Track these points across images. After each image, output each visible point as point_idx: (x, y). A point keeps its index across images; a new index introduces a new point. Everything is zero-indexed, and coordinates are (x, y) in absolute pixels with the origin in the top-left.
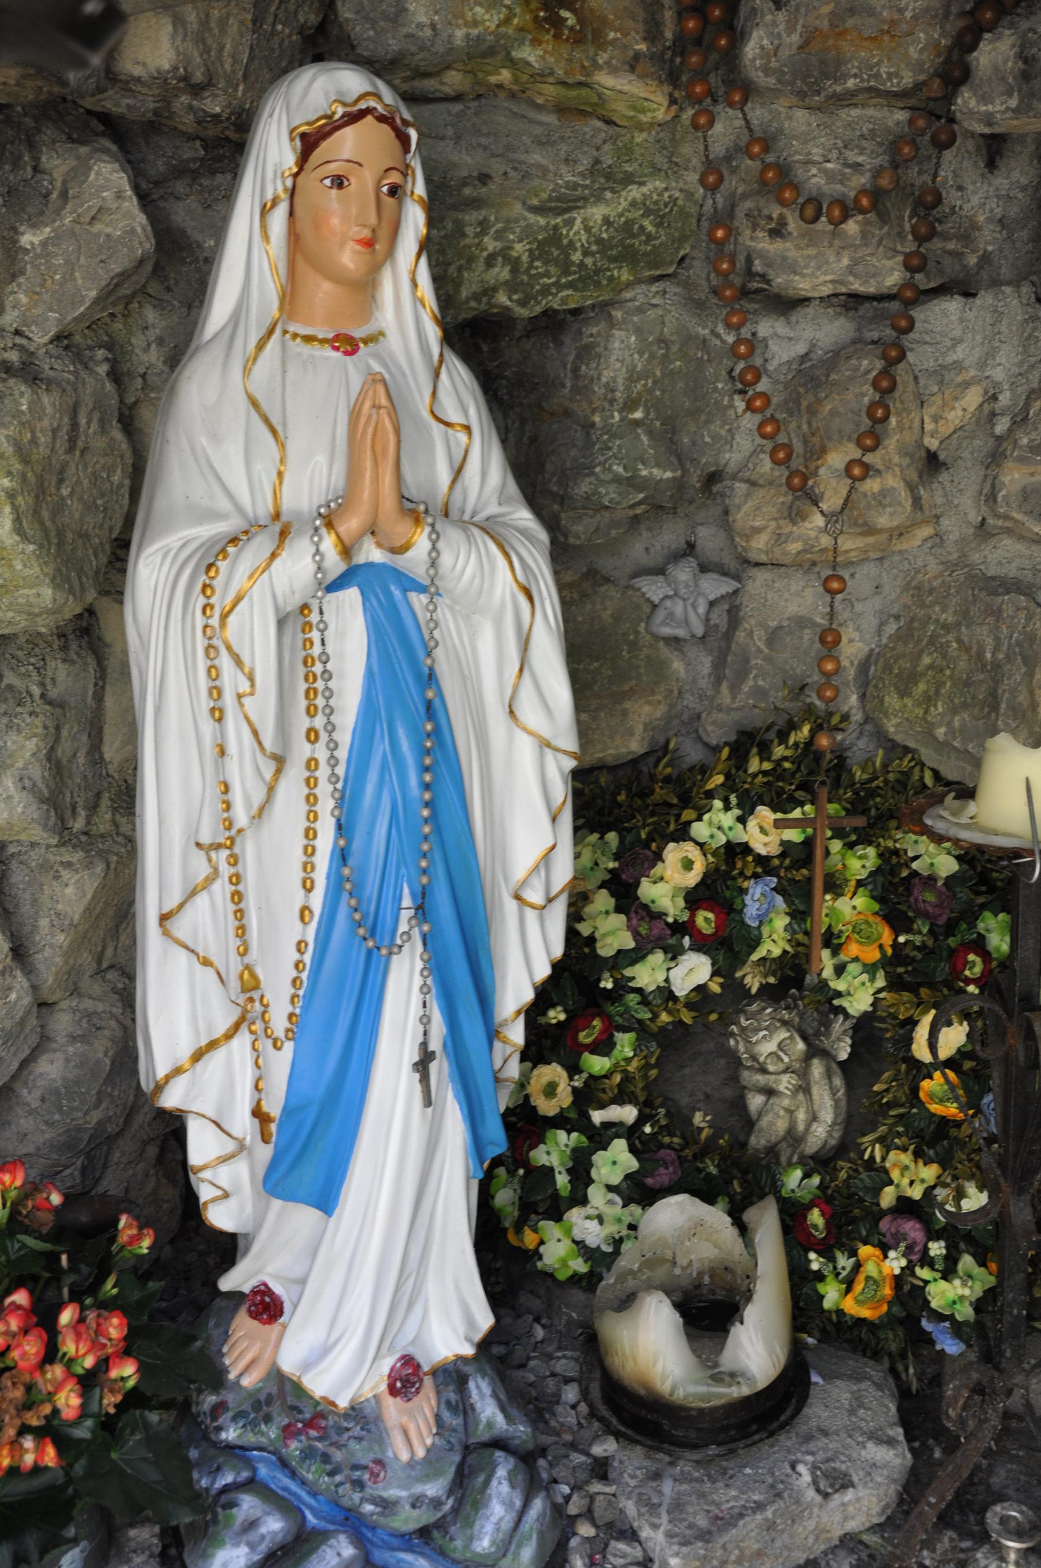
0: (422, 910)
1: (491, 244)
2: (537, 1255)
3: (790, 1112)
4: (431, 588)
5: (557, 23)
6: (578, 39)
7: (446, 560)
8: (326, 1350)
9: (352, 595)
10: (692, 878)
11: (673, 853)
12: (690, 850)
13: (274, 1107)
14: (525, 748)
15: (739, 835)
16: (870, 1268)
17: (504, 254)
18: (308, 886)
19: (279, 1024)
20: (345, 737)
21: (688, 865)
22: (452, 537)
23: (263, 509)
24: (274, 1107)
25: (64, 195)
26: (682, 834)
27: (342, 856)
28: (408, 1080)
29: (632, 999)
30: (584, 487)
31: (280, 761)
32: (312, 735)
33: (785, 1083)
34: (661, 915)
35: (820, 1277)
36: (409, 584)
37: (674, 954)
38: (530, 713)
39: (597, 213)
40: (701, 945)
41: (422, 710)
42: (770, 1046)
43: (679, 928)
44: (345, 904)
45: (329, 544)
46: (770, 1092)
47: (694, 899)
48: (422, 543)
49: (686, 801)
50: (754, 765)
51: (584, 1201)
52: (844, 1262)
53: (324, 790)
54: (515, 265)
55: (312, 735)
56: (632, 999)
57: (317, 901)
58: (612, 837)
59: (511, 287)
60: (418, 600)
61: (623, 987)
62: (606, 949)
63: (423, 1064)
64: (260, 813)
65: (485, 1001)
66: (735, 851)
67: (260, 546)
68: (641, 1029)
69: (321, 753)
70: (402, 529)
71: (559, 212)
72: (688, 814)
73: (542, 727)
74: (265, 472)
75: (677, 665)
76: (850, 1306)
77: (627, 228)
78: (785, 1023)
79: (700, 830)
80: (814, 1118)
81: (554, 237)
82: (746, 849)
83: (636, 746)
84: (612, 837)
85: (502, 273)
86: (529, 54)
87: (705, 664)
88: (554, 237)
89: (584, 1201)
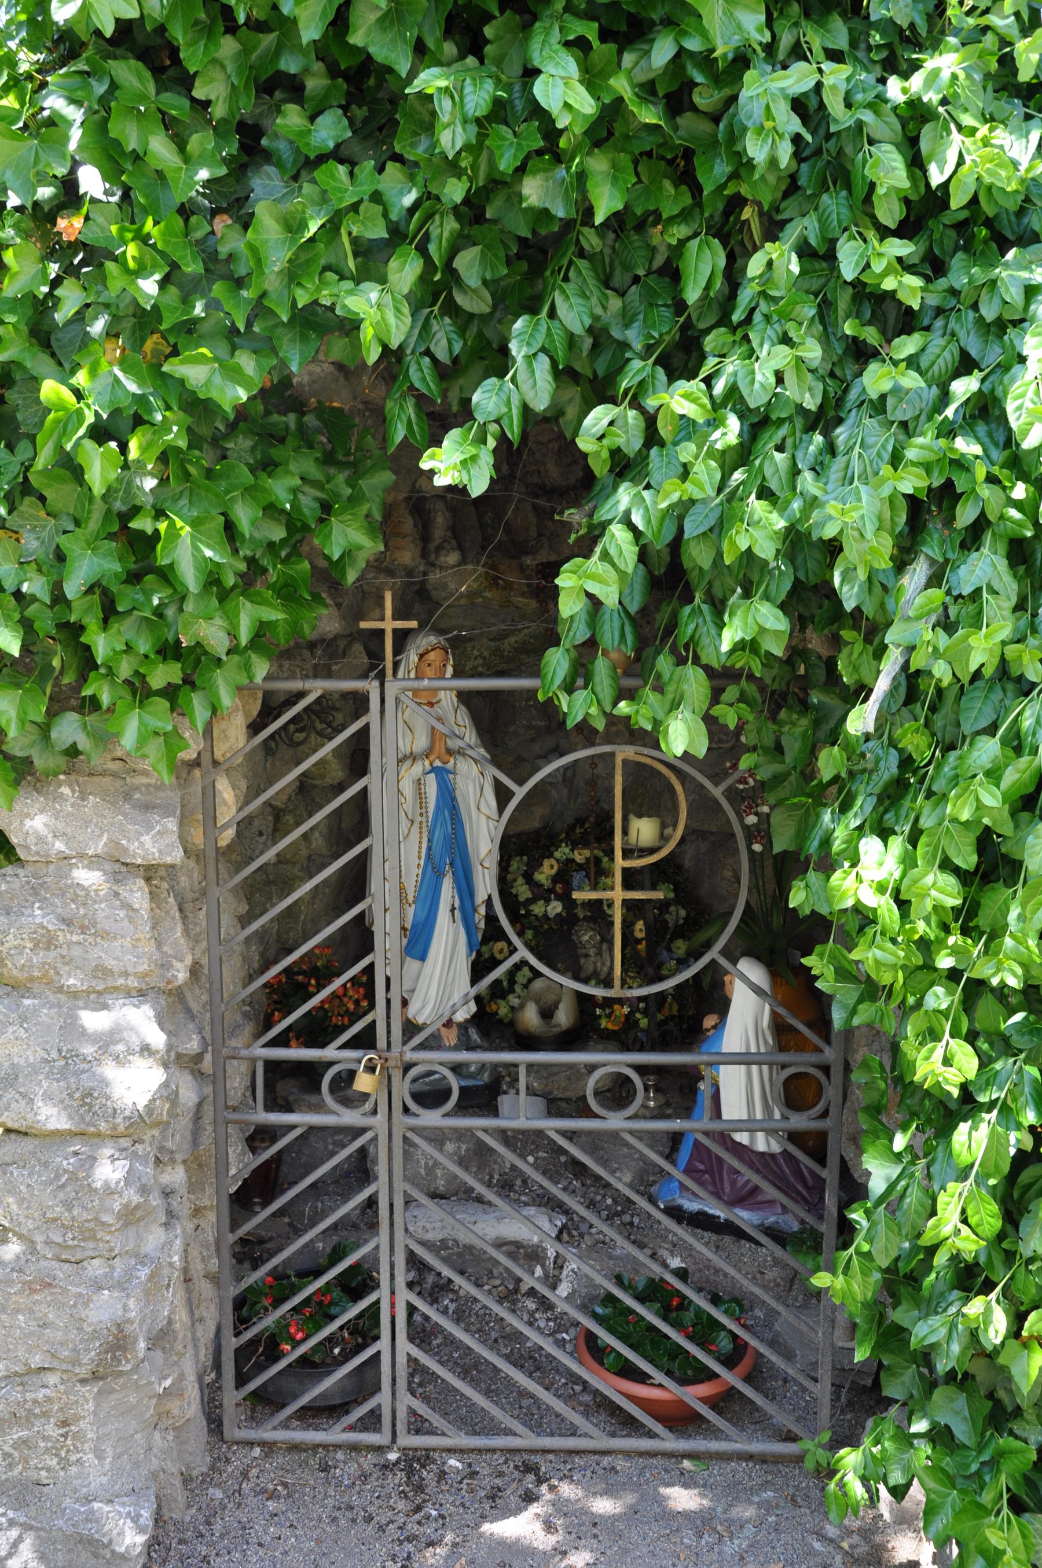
0: (451, 864)
1: (476, 653)
2: (496, 1013)
3: (595, 963)
4: (454, 773)
5: (497, 584)
6: (504, 588)
7: (458, 765)
8: (423, 1007)
9: (433, 775)
10: (554, 872)
11: (546, 863)
12: (553, 861)
13: (408, 926)
14: (483, 818)
15: (571, 856)
16: (617, 1013)
17: (481, 656)
18: (419, 858)
19: (411, 899)
20: (430, 815)
21: (552, 867)
22: (460, 758)
23: (408, 752)
24: (408, 926)
25: (344, 653)
26: (551, 856)
27: (429, 849)
28: (448, 914)
29: (533, 918)
30: (512, 728)
31: (412, 822)
32: (421, 815)
33: (592, 952)
34: (542, 885)
35: (600, 1017)
36: (449, 772)
37: (548, 901)
38: (484, 809)
39: (512, 639)
40: (558, 898)
41: (923, 840)
42: (586, 938)
43: (551, 891)
44: (430, 869)
45: (427, 763)
46: (587, 956)
47: (555, 879)
48: (452, 760)
49: (552, 844)
50: (578, 830)
51: (513, 991)
52: (608, 1011)
53: (425, 830)
54: (484, 658)
55: (421, 815)
56: (533, 918)
57: (422, 862)
58: (525, 858)
59: (483, 665)
60: (451, 776)
61: (529, 913)
62: (522, 899)
63: (453, 910)
64: (406, 837)
65: (472, 895)
66: (570, 861)
67: (409, 762)
68: (535, 928)
69: (424, 819)
70: (446, 757)
71: (499, 640)
72: (553, 849)
73: (487, 812)
74: (408, 741)
75: (554, 793)
76: (610, 1026)
77: (524, 642)
78: (592, 929)
79: (557, 854)
80: (603, 964)
81: (498, 649)
82: (573, 860)
83: (537, 824)
84: (525, 858)
85: (480, 661)
86: (488, 594)
87: (565, 792)
88: (498, 649)
89: (513, 991)
